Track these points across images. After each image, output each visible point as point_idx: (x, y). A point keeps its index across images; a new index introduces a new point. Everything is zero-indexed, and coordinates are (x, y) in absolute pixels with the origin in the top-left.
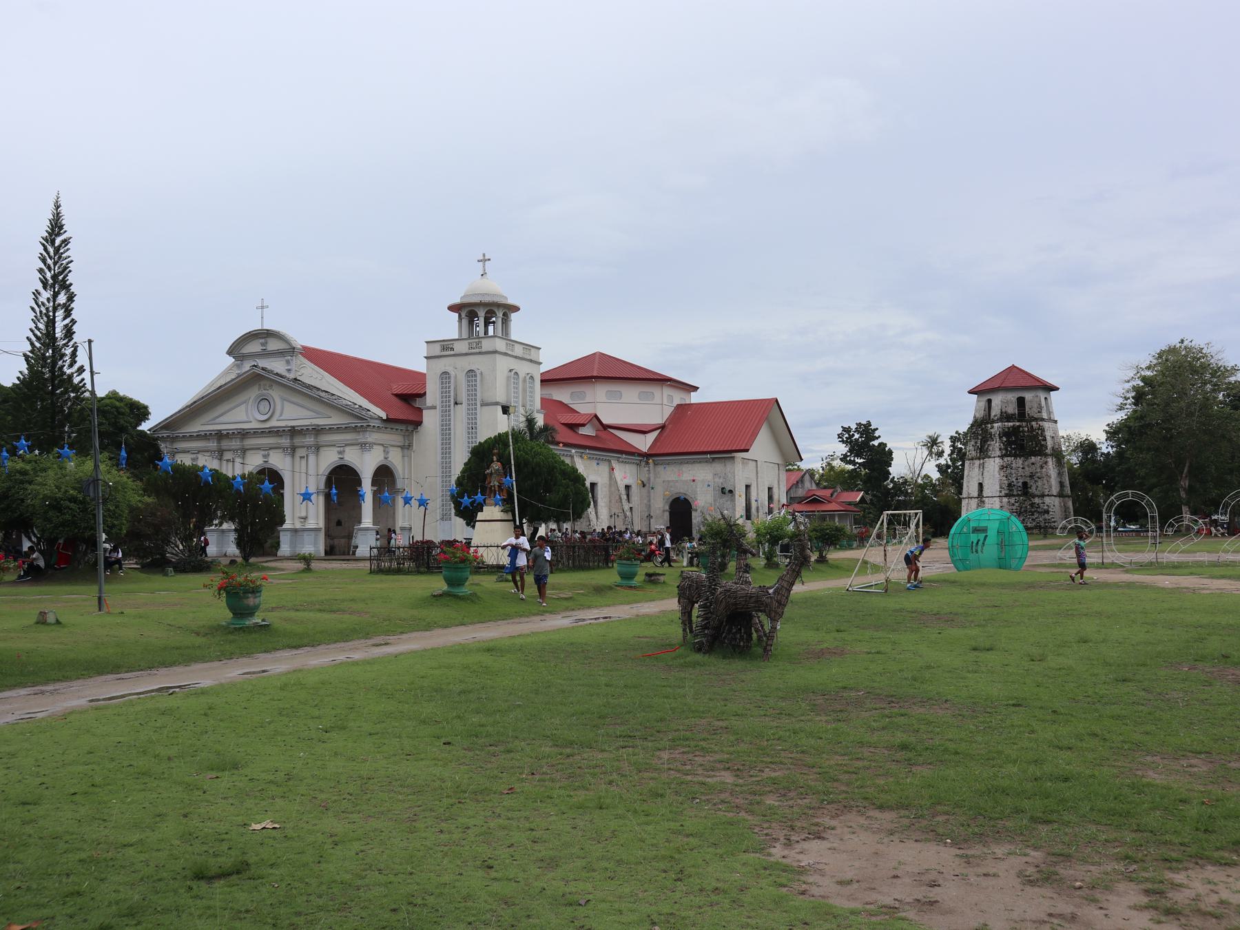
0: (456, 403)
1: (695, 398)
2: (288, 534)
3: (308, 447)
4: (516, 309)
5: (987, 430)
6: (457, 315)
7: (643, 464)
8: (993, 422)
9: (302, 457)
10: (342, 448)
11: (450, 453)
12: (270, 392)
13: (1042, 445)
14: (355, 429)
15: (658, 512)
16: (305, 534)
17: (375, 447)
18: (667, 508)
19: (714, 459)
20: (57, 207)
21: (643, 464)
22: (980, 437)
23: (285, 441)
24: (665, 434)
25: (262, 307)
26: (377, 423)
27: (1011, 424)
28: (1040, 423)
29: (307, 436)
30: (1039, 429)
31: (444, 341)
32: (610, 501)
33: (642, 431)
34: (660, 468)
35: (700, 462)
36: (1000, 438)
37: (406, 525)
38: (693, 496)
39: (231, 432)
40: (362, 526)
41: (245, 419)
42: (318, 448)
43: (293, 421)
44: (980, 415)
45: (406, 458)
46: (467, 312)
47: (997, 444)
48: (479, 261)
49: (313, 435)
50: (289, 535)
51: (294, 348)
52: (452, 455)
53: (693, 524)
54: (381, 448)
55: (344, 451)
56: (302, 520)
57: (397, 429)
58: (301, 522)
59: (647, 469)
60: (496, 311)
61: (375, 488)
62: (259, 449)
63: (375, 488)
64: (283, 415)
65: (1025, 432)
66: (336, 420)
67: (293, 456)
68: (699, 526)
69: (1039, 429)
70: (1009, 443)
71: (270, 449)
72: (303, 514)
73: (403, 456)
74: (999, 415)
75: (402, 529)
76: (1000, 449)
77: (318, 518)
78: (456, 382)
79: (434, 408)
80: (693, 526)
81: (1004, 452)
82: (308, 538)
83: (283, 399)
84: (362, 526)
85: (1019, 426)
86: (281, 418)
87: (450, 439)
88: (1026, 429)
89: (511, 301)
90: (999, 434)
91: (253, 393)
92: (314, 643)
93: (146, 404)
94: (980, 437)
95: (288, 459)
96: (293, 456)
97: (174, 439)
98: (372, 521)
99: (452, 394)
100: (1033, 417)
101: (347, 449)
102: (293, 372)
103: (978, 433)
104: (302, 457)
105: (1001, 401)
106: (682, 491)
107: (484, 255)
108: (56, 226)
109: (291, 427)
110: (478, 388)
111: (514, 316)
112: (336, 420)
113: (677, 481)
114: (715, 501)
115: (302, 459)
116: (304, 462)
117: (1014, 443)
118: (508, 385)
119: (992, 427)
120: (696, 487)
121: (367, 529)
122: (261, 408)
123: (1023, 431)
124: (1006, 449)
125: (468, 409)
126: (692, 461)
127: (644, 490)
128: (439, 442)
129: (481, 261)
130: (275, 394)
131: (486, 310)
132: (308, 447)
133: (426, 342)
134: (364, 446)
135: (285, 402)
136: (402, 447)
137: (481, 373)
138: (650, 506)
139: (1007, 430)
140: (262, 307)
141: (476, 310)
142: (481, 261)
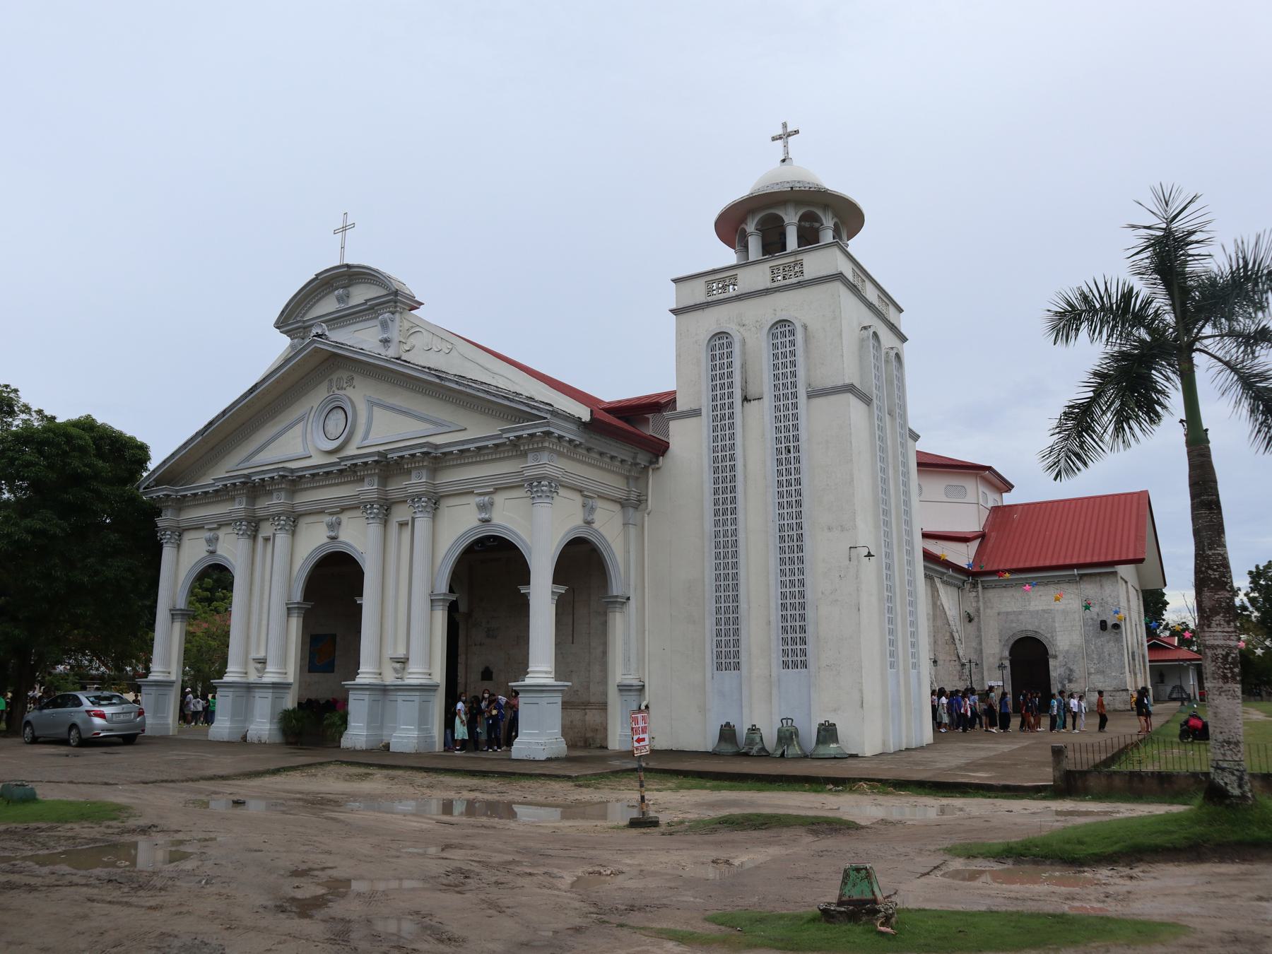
0: (746, 399)
1: (1008, 499)
2: (366, 696)
3: (415, 498)
6: (671, 422)
7: (967, 586)
9: (402, 525)
10: (487, 498)
11: (734, 511)
14: (515, 448)
15: (991, 659)
16: (400, 697)
17: (562, 491)
18: (1007, 653)
19: (1082, 576)
21: (967, 586)
23: (369, 489)
24: (990, 545)
25: (344, 229)
26: (569, 432)
29: (414, 473)
31: (714, 272)
32: (935, 642)
33: (963, 539)
34: (991, 594)
35: (1058, 583)
37: (631, 680)
38: (1049, 635)
39: (267, 477)
40: (528, 681)
41: (300, 451)
42: (435, 501)
45: (632, 530)
46: (756, 225)
48: (774, 139)
49: (424, 472)
50: (366, 698)
51: (396, 293)
52: (740, 516)
53: (1052, 678)
54: (578, 499)
55: (492, 504)
56: (398, 665)
57: (612, 458)
58: (396, 670)
59: (974, 594)
60: (820, 214)
61: (562, 590)
62: (321, 512)
63: (562, 590)
66: (478, 429)
67: (385, 523)
68: (1061, 683)
71: (344, 510)
72: (401, 652)
73: (625, 524)
75: (624, 689)
77: (430, 663)
78: (744, 353)
79: (696, 413)
80: (1052, 682)
82: (406, 708)
83: (372, 404)
84: (528, 681)
87: (733, 478)
91: (317, 398)
92: (629, 560)
93: (84, 414)
95: (374, 529)
96: (385, 523)
97: (181, 503)
98: (553, 669)
99: (737, 378)
101: (499, 499)
104: (402, 525)
106: (1030, 628)
107: (785, 125)
109: (379, 453)
110: (800, 359)
112: (478, 429)
113: (1021, 613)
114: (1087, 641)
115: (404, 529)
116: (406, 533)
118: (861, 359)
120: (1054, 622)
121: (541, 689)
125: (777, 408)
126: (1046, 581)
127: (971, 628)
128: (708, 487)
130: (359, 394)
131: (800, 213)
132: (415, 498)
133: (676, 281)
134: (536, 486)
135: (375, 408)
136: (623, 504)
137: (805, 327)
138: (981, 650)
140: (344, 229)
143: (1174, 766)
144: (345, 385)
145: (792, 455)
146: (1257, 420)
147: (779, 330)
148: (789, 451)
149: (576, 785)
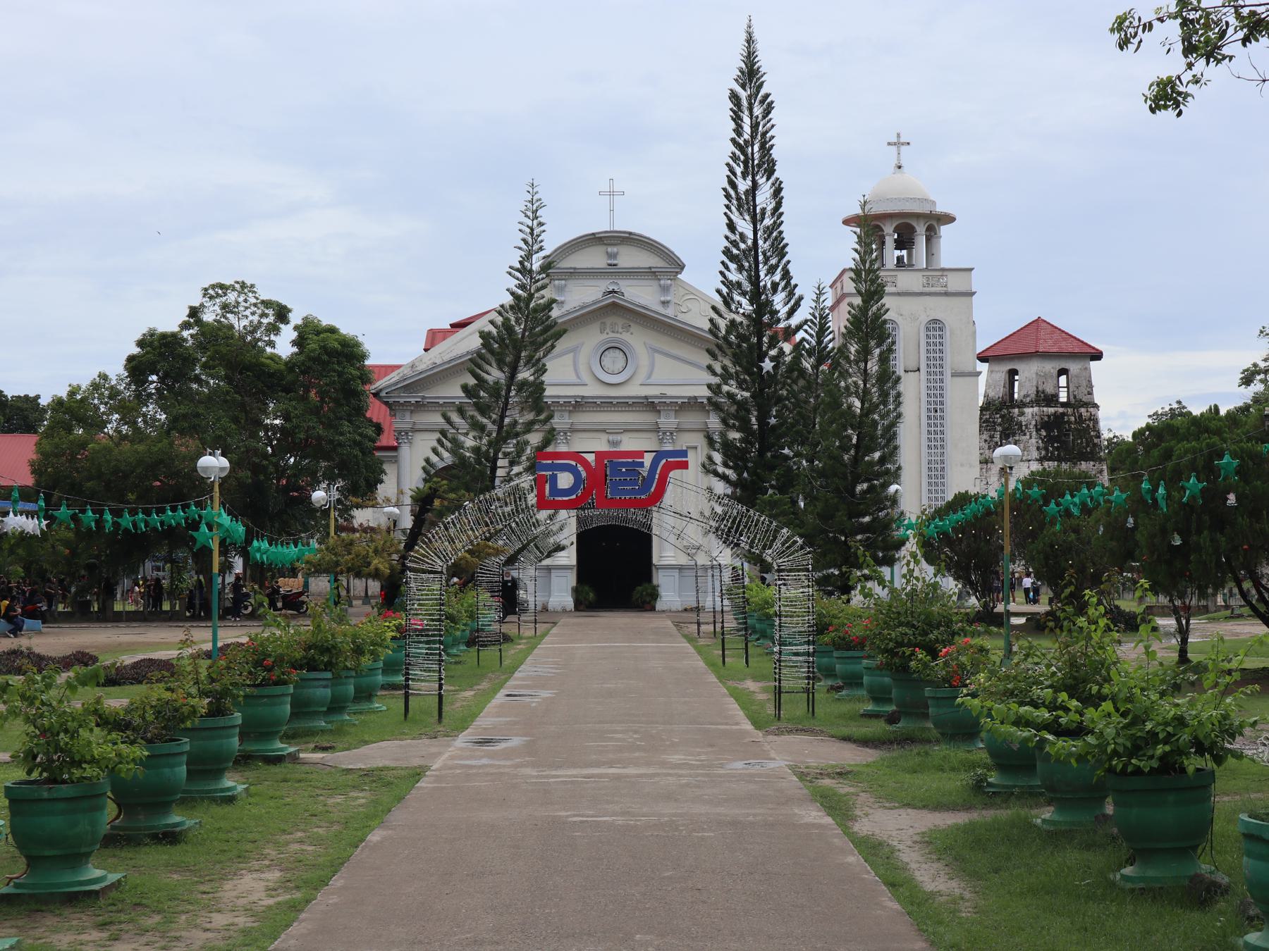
4: (949, 219)
5: (1012, 418)
8: (1022, 405)
12: (626, 337)
13: (1095, 445)
20: (750, 41)
22: (999, 428)
27: (1051, 410)
28: (1092, 410)
30: (1090, 419)
36: (1038, 430)
41: (573, 379)
43: (575, 388)
44: (999, 392)
47: (1033, 441)
48: (889, 144)
64: (653, 377)
65: (1071, 423)
69: (1090, 419)
70: (1049, 440)
74: (1033, 396)
76: (1038, 448)
81: (1043, 453)
85: (1063, 414)
86: (649, 381)
88: (1073, 419)
89: (940, 208)
90: (1036, 425)
94: (999, 428)
100: (1081, 400)
102: (672, 306)
103: (994, 422)
105: (1037, 374)
107: (898, 135)
108: (750, 74)
109: (690, 398)
111: (944, 230)
117: (1056, 439)
119: (1022, 414)
122: (607, 361)
123: (1069, 422)
124: (1046, 449)
129: (895, 144)
130: (637, 340)
139: (1046, 419)
140: (612, 194)
141: (882, 225)
142: (895, 144)
143: (698, 629)
144: (620, 330)
145: (938, 414)
146: (1225, 479)
147: (932, 326)
148: (936, 411)
149: (1208, 619)
